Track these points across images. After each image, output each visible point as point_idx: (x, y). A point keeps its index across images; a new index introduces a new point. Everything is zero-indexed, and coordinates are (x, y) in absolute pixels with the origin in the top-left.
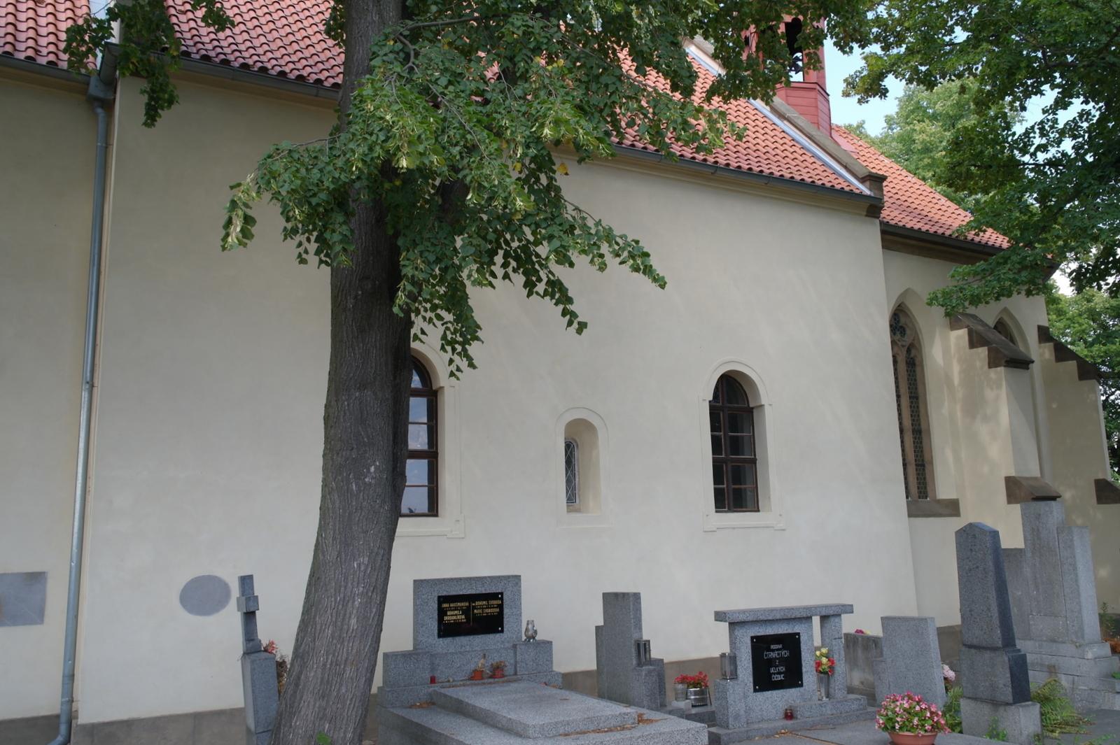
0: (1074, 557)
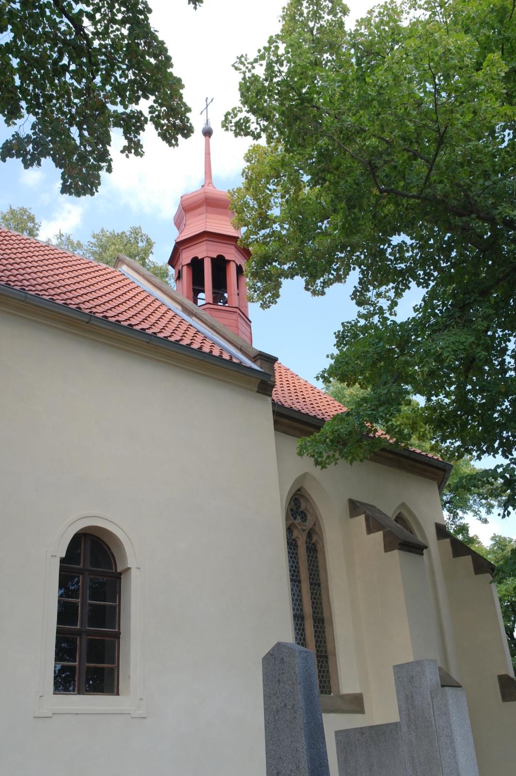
0: (450, 725)
